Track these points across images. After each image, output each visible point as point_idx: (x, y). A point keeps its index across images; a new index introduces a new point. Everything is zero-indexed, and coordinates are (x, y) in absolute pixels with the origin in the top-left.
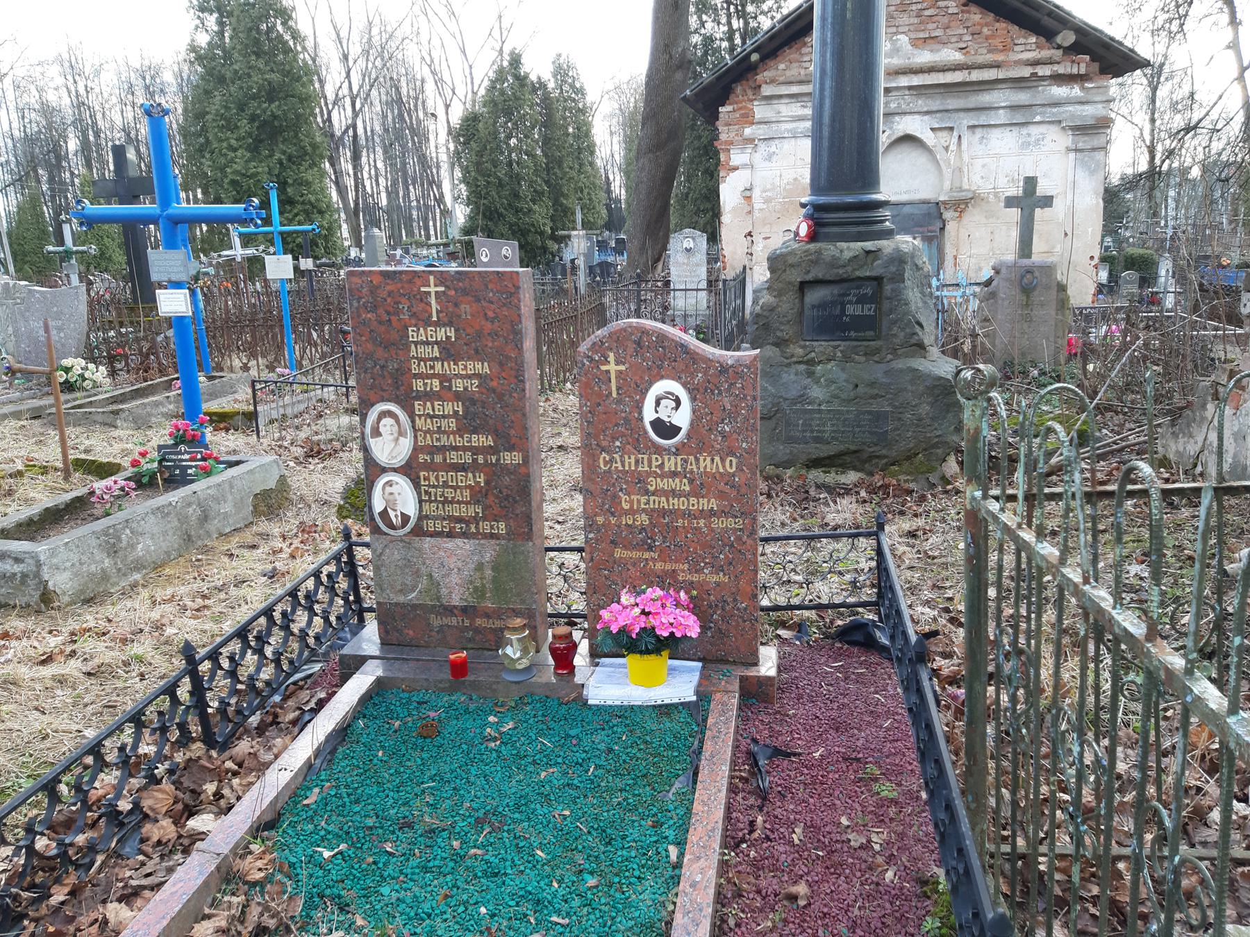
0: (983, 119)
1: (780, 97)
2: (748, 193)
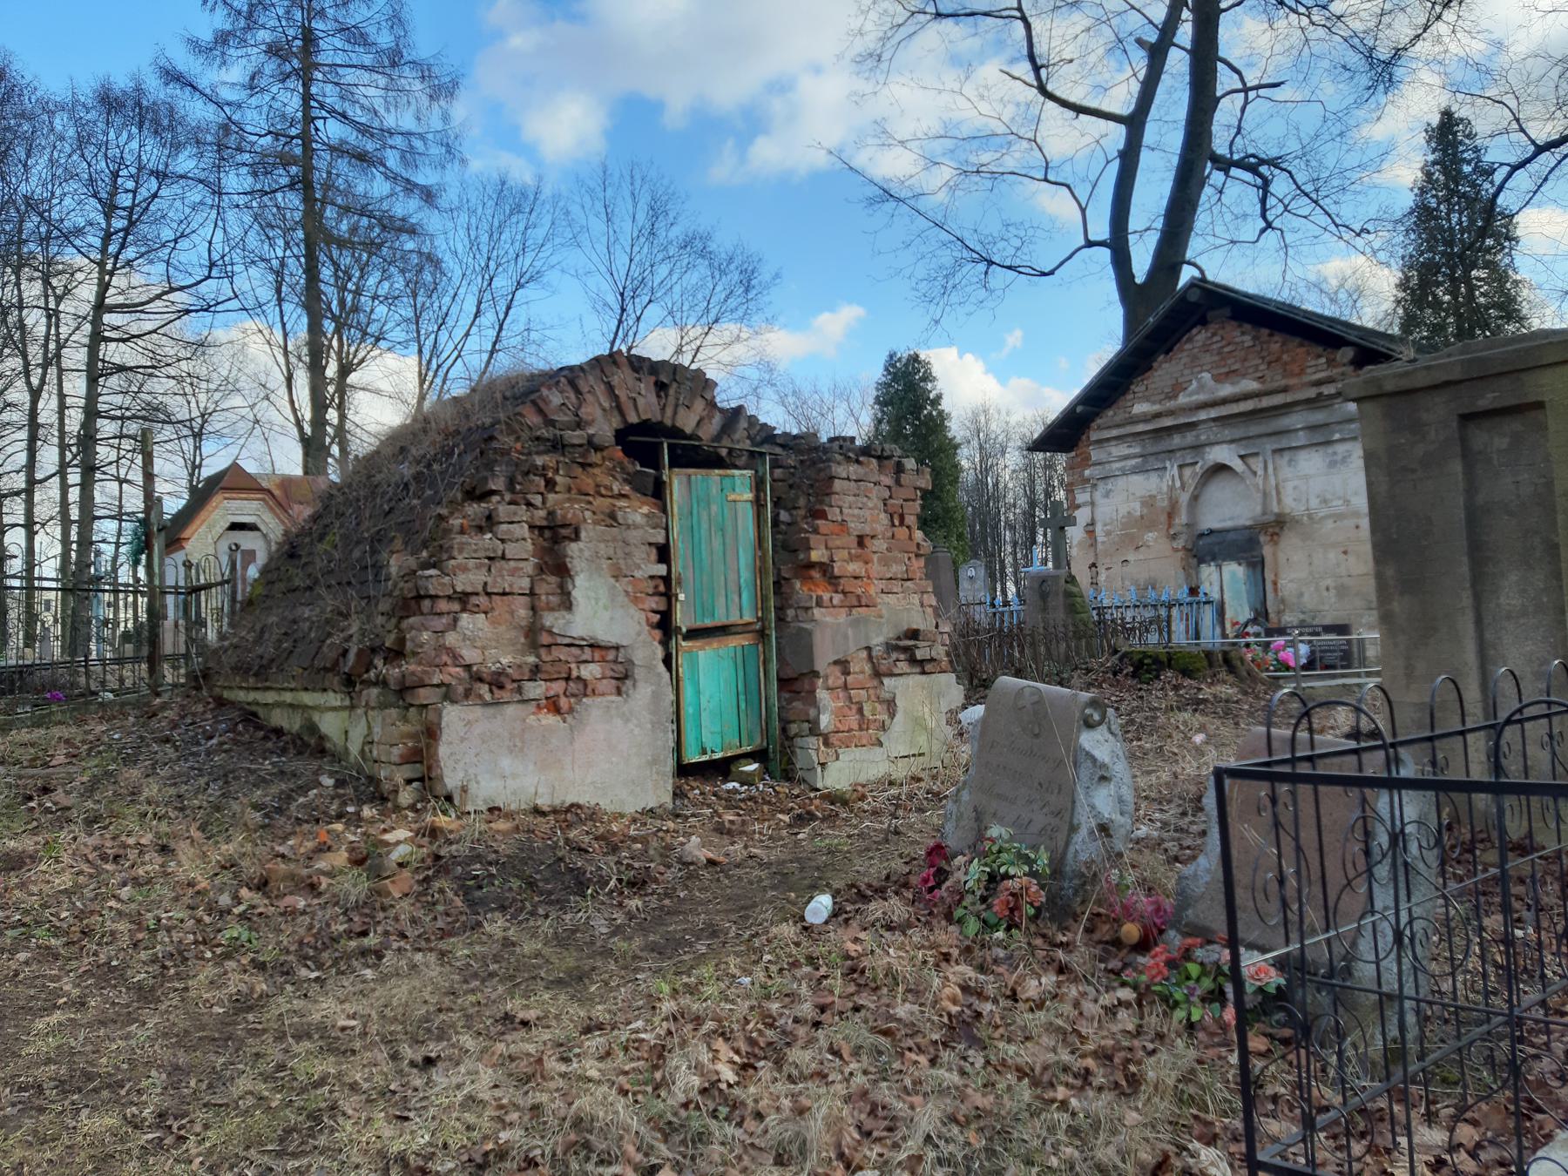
0: (1284, 443)
1: (1108, 440)
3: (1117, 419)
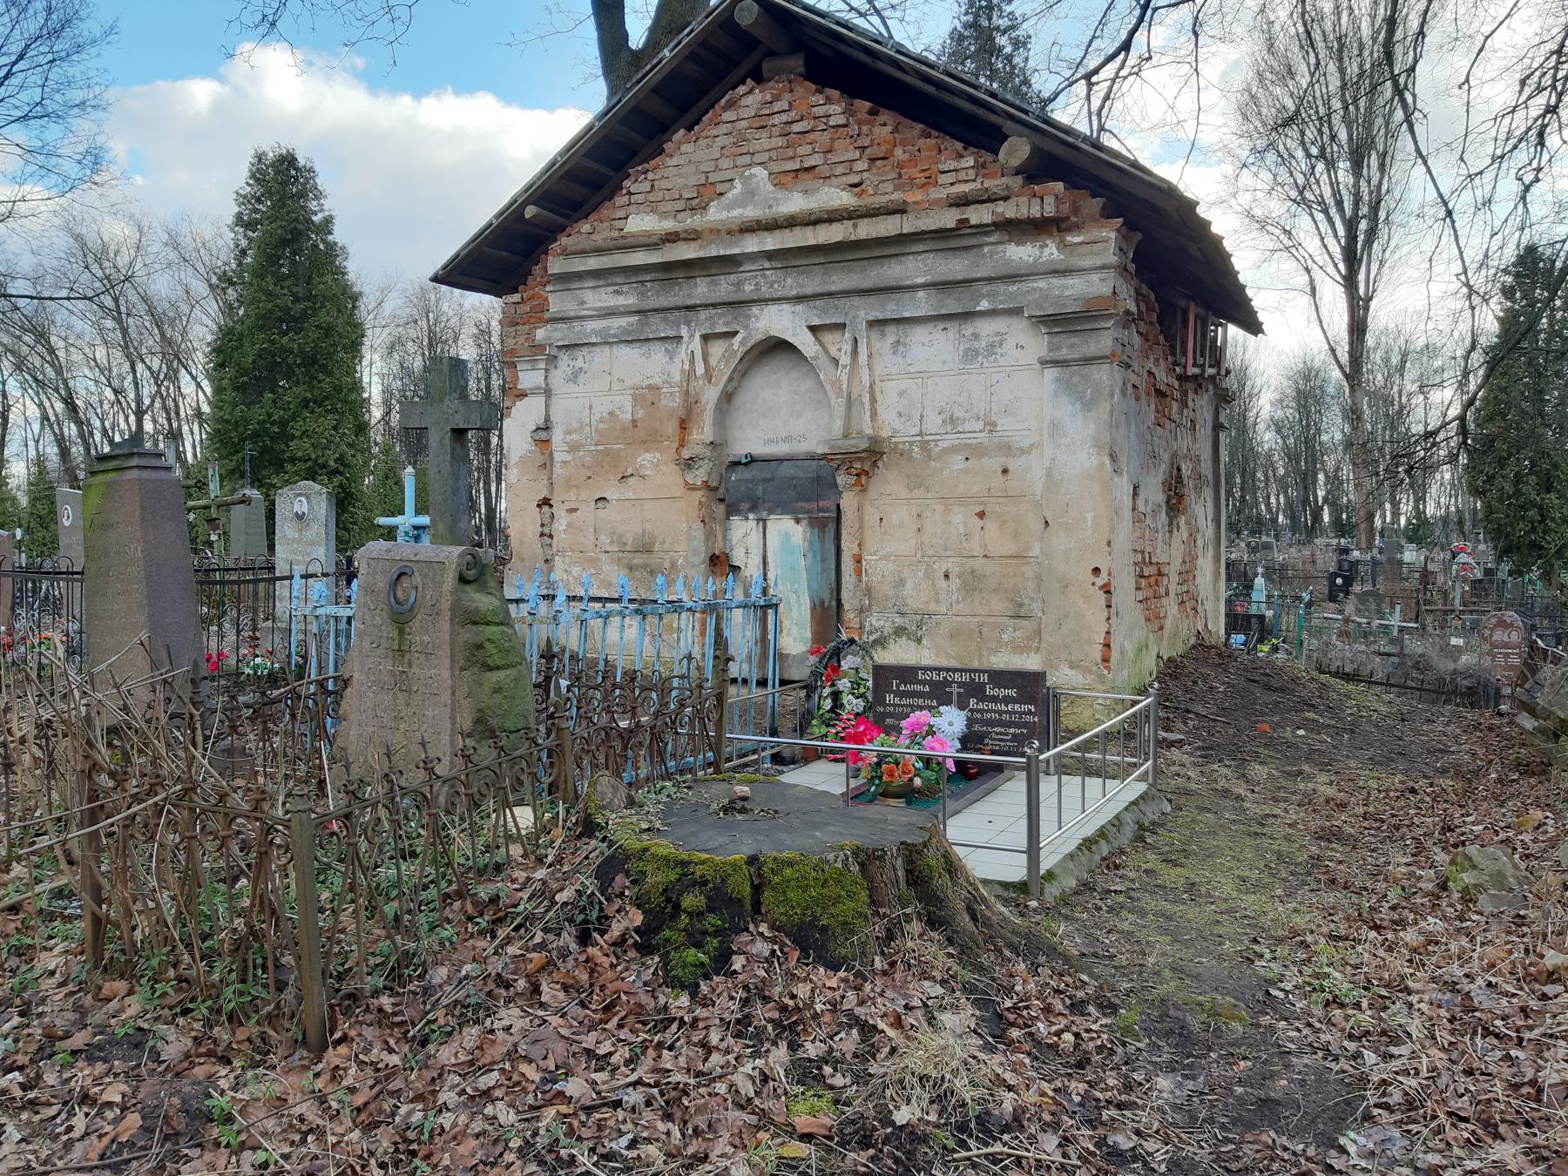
1: (579, 276)
2: (543, 435)
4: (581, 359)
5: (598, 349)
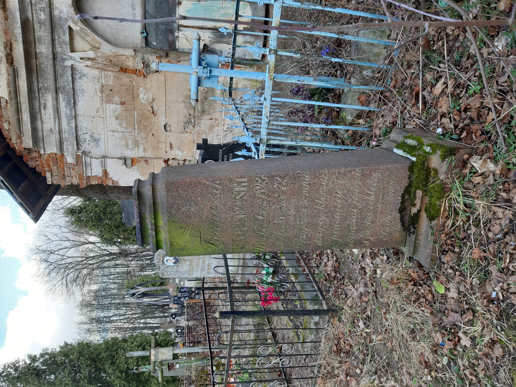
1: (34, 130)
2: (129, 162)
3: (13, 119)
4: (84, 136)
5: (79, 124)
